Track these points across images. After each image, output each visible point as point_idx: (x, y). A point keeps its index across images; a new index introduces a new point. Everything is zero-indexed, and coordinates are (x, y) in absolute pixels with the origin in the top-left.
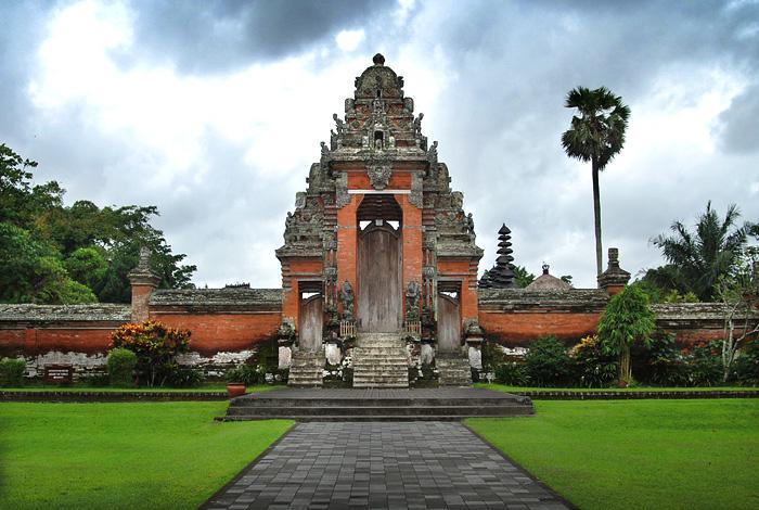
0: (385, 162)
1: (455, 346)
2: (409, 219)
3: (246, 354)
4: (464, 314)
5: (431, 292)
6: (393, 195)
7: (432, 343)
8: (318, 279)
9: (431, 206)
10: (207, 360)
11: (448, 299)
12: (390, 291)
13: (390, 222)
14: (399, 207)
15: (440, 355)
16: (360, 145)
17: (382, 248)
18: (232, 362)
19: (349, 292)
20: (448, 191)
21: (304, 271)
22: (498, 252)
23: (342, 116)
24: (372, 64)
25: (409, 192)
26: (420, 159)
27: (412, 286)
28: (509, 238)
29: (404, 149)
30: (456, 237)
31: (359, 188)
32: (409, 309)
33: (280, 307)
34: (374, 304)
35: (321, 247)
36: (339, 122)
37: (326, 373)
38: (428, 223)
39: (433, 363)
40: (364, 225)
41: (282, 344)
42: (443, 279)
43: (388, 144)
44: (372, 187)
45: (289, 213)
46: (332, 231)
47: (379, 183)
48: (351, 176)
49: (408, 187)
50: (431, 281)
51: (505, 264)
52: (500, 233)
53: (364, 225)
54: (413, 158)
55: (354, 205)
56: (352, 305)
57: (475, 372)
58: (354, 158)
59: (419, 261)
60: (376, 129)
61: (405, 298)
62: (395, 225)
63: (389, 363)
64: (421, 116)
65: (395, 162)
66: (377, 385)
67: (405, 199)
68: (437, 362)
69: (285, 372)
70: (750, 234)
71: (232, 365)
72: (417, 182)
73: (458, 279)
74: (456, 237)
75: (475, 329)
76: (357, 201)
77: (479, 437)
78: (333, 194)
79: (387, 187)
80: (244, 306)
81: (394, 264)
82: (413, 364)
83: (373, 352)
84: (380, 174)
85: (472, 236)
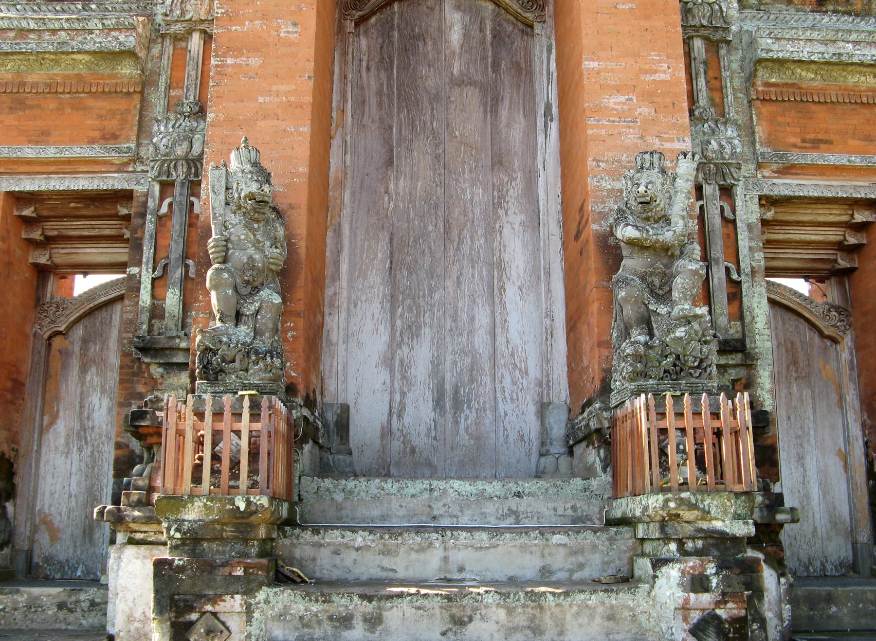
8: (115, 182)
12: (497, 266)
21: (42, 137)
32: (646, 322)
34: (413, 330)
50: (727, 192)
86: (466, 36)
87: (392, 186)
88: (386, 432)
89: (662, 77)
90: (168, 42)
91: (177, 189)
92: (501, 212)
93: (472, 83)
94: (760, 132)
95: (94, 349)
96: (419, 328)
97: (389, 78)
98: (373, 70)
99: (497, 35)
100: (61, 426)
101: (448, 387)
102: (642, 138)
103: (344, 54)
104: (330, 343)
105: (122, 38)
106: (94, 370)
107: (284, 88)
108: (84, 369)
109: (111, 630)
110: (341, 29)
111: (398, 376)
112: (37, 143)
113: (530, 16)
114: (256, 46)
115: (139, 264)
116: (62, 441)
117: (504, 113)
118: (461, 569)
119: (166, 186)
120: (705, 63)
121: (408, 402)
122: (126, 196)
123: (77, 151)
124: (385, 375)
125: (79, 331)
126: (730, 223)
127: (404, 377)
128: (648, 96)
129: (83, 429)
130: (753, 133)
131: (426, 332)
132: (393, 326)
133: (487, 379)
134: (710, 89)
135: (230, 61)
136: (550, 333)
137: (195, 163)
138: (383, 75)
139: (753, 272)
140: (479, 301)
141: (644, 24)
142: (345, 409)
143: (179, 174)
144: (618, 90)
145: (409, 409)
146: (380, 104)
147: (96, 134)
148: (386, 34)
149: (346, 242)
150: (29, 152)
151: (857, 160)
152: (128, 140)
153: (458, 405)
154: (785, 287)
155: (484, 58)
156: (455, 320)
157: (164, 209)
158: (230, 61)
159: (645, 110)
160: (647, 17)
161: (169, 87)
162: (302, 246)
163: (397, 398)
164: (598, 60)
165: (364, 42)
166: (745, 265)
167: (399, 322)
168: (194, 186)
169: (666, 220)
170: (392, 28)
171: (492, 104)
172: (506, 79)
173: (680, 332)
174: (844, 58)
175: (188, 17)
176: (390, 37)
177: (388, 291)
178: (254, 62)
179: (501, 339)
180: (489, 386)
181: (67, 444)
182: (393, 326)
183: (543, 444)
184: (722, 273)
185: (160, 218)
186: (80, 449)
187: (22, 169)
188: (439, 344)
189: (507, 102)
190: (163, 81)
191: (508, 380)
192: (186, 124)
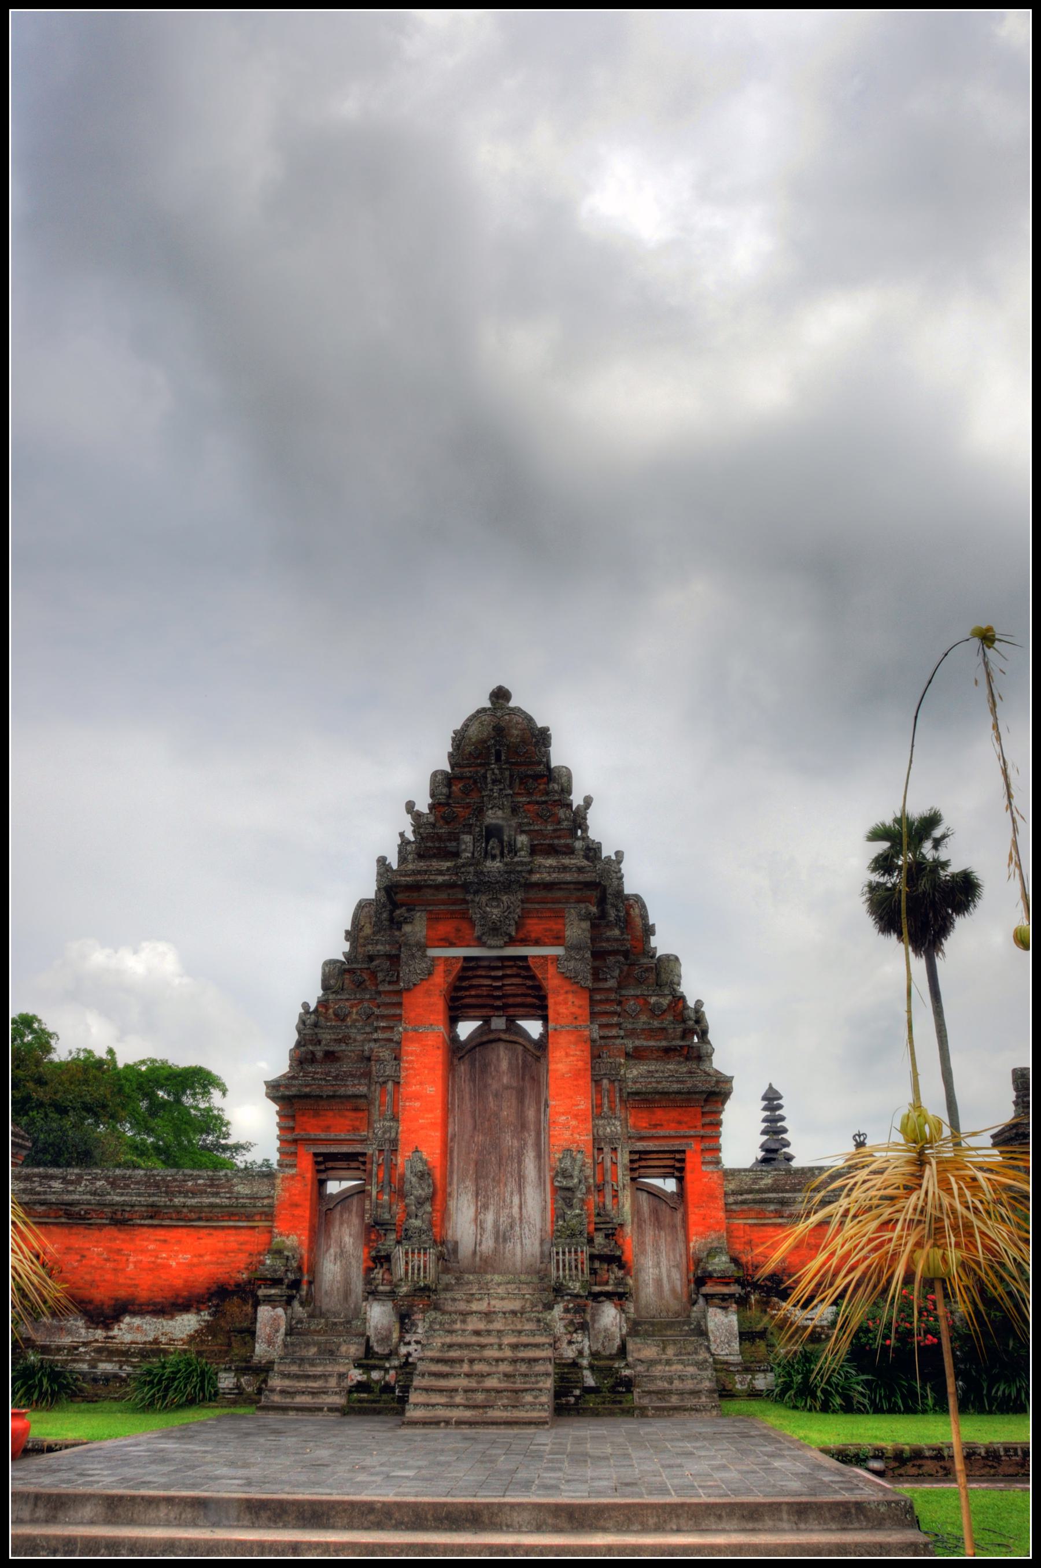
0: (507, 887)
1: (674, 1305)
2: (562, 1010)
3: (186, 1324)
4: (693, 1230)
5: (615, 1175)
6: (524, 958)
7: (619, 1297)
8: (358, 1148)
9: (611, 983)
10: (100, 1334)
11: (655, 1194)
13: (519, 1022)
14: (539, 988)
15: (635, 1328)
16: (456, 855)
17: (505, 1080)
18: (156, 1341)
19: (422, 1176)
20: (650, 953)
22: (765, 1120)
23: (423, 805)
24: (487, 704)
25: (558, 951)
26: (582, 878)
27: (567, 1163)
28: (780, 1107)
29: (550, 862)
30: (668, 1051)
31: (452, 945)
32: (563, 1216)
33: (269, 1215)
34: (485, 1207)
35: (367, 1075)
36: (417, 816)
37: (356, 1375)
38: (604, 1020)
39: (622, 1351)
40: (466, 1029)
41: (269, 1300)
42: (640, 1146)
43: (514, 851)
44: (480, 943)
45: (305, 1005)
46: (390, 1040)
47: (495, 930)
48: (434, 919)
49: (558, 940)
51: (776, 1151)
52: (764, 1098)
53: (466, 1029)
54: (568, 877)
55: (440, 980)
56: (428, 1208)
57: (721, 1367)
58: (440, 879)
59: (583, 1104)
60: (488, 821)
61: (556, 1190)
62: (534, 1028)
63: (508, 1353)
64: (588, 801)
65: (529, 886)
66: (468, 1414)
67: (551, 970)
68: (630, 1347)
69: (263, 1370)
70: (366, 1299)
71: (153, 1350)
72: (576, 930)
73: (676, 1145)
74: (668, 1051)
75: (720, 1263)
76: (447, 972)
77: (521, 1215)
78: (394, 959)
79: (512, 942)
80: (192, 1208)
81: (531, 1114)
82: (570, 1353)
83: (474, 1323)
84: (495, 913)
85: (705, 1048)
86: (510, 1063)
87: (476, 1139)
88: (475, 1253)
89: (582, 1107)
90: (378, 1085)
91: (386, 1153)
92: (525, 1151)
93: (512, 1088)
94: (630, 1121)
95: (345, 1216)
96: (488, 1205)
97: (475, 1086)
98: (467, 1083)
99: (524, 1061)
100: (332, 1251)
101: (501, 1234)
102: (572, 1135)
103: (453, 1076)
104: (450, 1214)
105: (361, 1089)
106: (346, 1225)
107: (430, 1116)
108: (341, 1224)
109: (368, 1334)
110: (452, 1063)
111: (479, 1227)
112: (326, 1131)
113: (538, 1054)
114: (417, 1097)
115: (371, 1185)
116: (332, 1258)
117: (527, 1102)
118: (494, 1307)
119: (381, 1151)
120: (608, 1091)
121: (484, 1239)
122: (364, 1154)
123: (343, 1136)
124: (473, 1227)
125: (339, 1208)
126: (614, 1164)
127: (481, 1228)
128: (575, 1116)
129: (342, 1251)
130: (627, 1122)
131: (492, 1208)
132: (477, 1205)
133: (518, 1229)
134: (609, 1102)
135: (407, 1104)
136: (544, 1208)
137: (394, 1142)
138: (471, 1084)
139: (624, 1185)
140: (515, 1193)
141: (575, 1083)
142: (456, 1243)
143: (386, 1147)
144: (563, 1114)
145: (484, 1242)
146: (471, 1099)
147: (351, 1128)
148: (473, 1064)
149: (455, 1168)
150: (323, 1135)
151: (673, 1133)
152: (364, 1131)
153: (505, 1240)
154: (653, 1185)
155: (518, 1075)
156: (504, 1202)
157: (380, 1161)
158: (407, 1104)
159: (574, 1123)
160: (576, 1080)
161: (380, 1106)
162: (438, 1186)
163: (479, 1237)
164: (556, 1100)
165: (462, 1067)
166: (621, 1184)
167: (479, 1203)
168: (394, 1151)
169: (571, 1177)
170: (475, 1060)
171: (521, 1100)
172: (528, 1085)
173: (574, 1221)
174: (666, 1090)
175: (387, 1074)
176: (475, 1064)
177: (475, 1189)
178: (417, 1104)
179: (524, 1211)
180: (518, 1233)
181: (335, 1259)
182: (477, 1205)
183: (541, 1258)
184: (610, 1187)
185: (379, 1165)
186: (341, 1261)
187: (319, 1142)
188: (497, 1214)
189: (528, 1097)
190: (377, 1103)
191: (527, 1228)
192: (388, 1124)
